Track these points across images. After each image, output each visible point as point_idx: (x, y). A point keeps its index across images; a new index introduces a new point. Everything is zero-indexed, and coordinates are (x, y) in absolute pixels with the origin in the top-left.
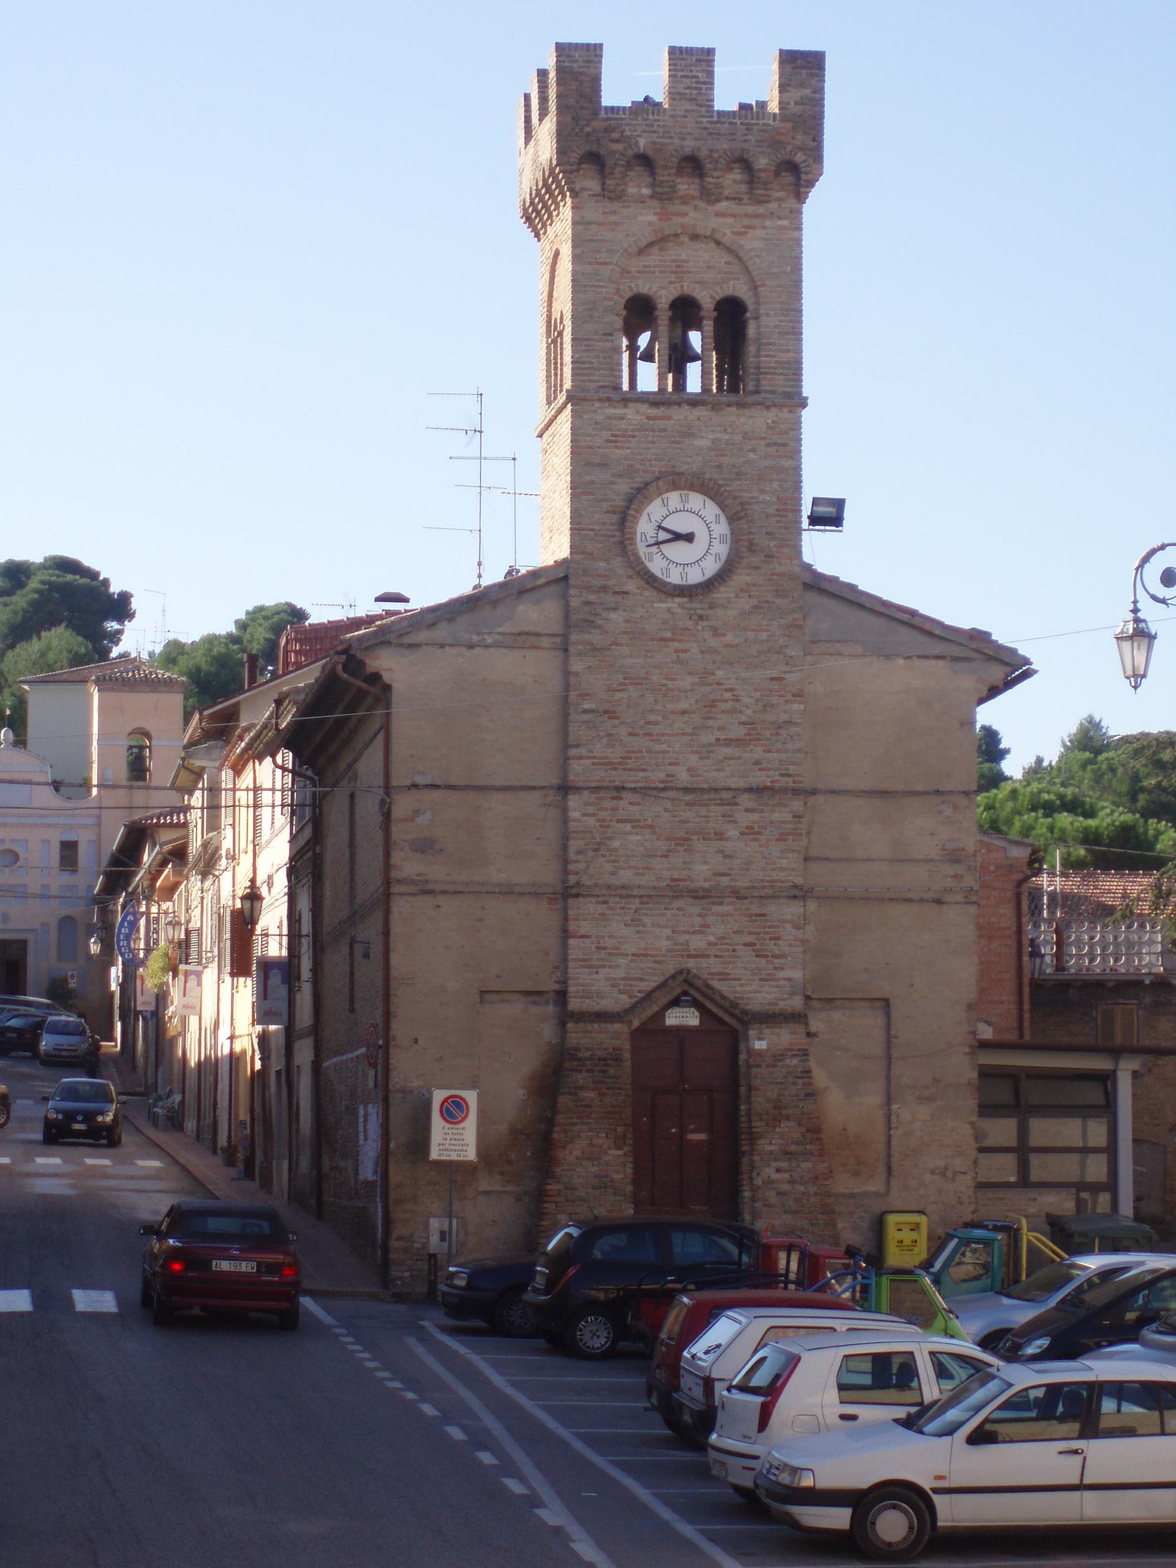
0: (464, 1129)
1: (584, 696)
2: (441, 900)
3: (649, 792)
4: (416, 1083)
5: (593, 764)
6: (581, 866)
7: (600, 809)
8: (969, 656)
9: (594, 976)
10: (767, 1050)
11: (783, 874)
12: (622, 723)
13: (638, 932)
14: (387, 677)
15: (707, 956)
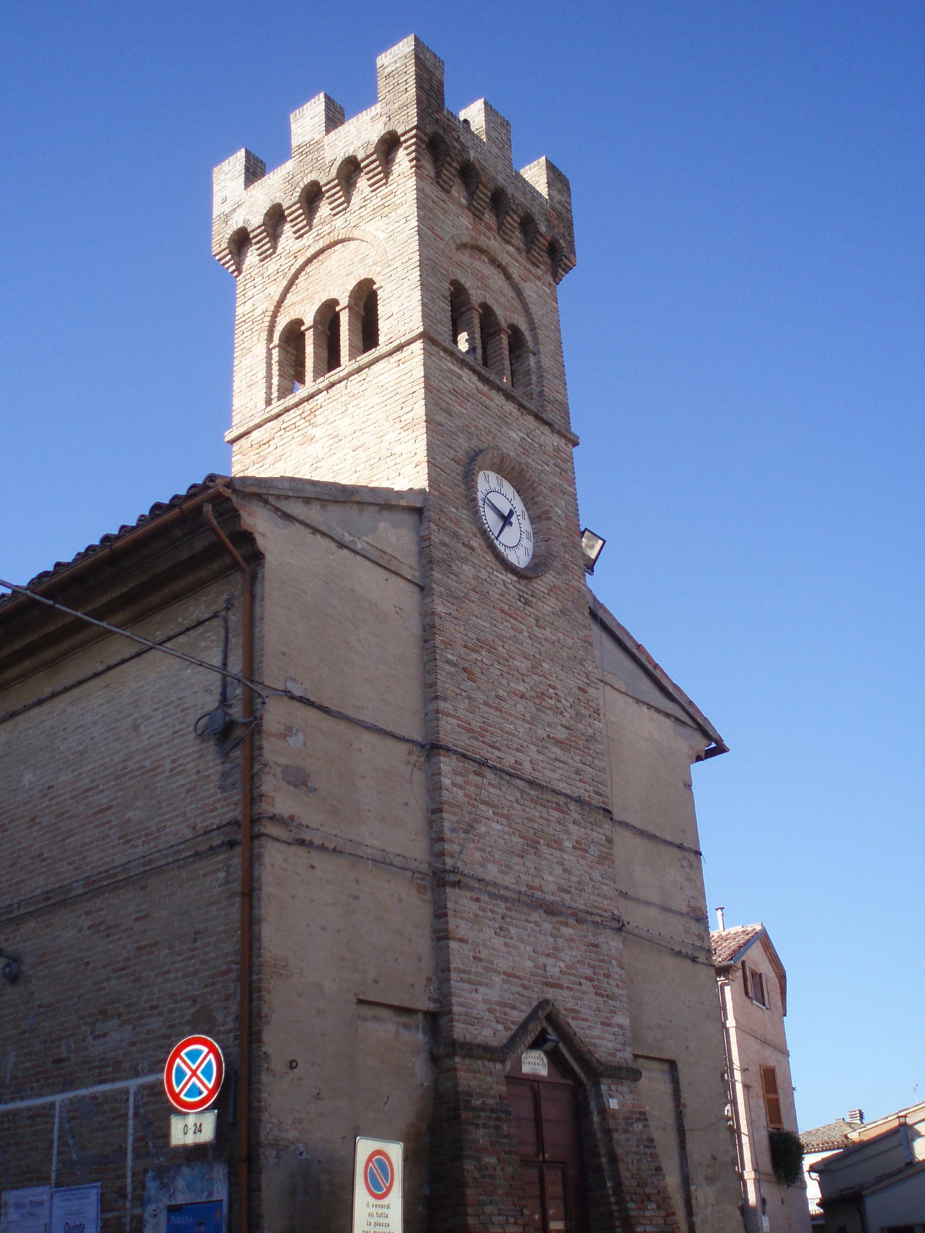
0: (388, 1207)
1: (449, 644)
2: (316, 858)
3: (503, 775)
4: (292, 1134)
5: (459, 726)
6: (456, 848)
7: (467, 783)
8: (682, 719)
9: (474, 995)
10: (619, 1110)
11: (605, 902)
12: (479, 688)
13: (506, 945)
14: (261, 542)
15: (560, 987)
